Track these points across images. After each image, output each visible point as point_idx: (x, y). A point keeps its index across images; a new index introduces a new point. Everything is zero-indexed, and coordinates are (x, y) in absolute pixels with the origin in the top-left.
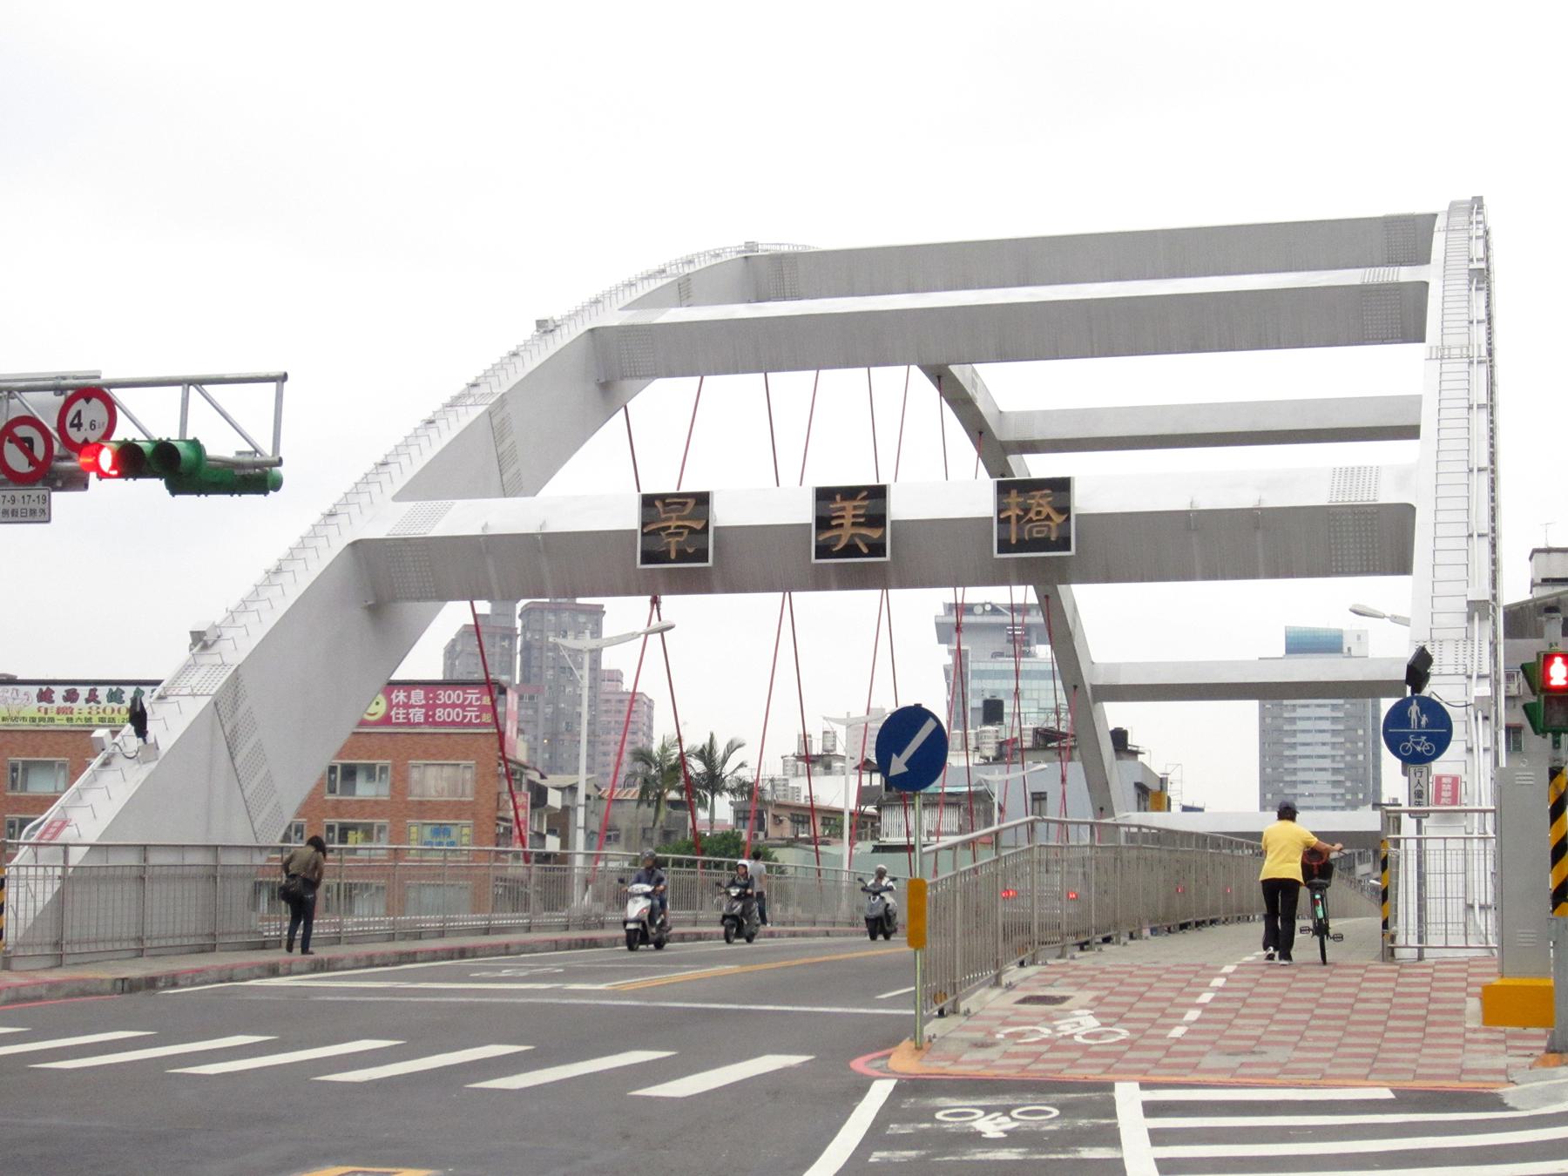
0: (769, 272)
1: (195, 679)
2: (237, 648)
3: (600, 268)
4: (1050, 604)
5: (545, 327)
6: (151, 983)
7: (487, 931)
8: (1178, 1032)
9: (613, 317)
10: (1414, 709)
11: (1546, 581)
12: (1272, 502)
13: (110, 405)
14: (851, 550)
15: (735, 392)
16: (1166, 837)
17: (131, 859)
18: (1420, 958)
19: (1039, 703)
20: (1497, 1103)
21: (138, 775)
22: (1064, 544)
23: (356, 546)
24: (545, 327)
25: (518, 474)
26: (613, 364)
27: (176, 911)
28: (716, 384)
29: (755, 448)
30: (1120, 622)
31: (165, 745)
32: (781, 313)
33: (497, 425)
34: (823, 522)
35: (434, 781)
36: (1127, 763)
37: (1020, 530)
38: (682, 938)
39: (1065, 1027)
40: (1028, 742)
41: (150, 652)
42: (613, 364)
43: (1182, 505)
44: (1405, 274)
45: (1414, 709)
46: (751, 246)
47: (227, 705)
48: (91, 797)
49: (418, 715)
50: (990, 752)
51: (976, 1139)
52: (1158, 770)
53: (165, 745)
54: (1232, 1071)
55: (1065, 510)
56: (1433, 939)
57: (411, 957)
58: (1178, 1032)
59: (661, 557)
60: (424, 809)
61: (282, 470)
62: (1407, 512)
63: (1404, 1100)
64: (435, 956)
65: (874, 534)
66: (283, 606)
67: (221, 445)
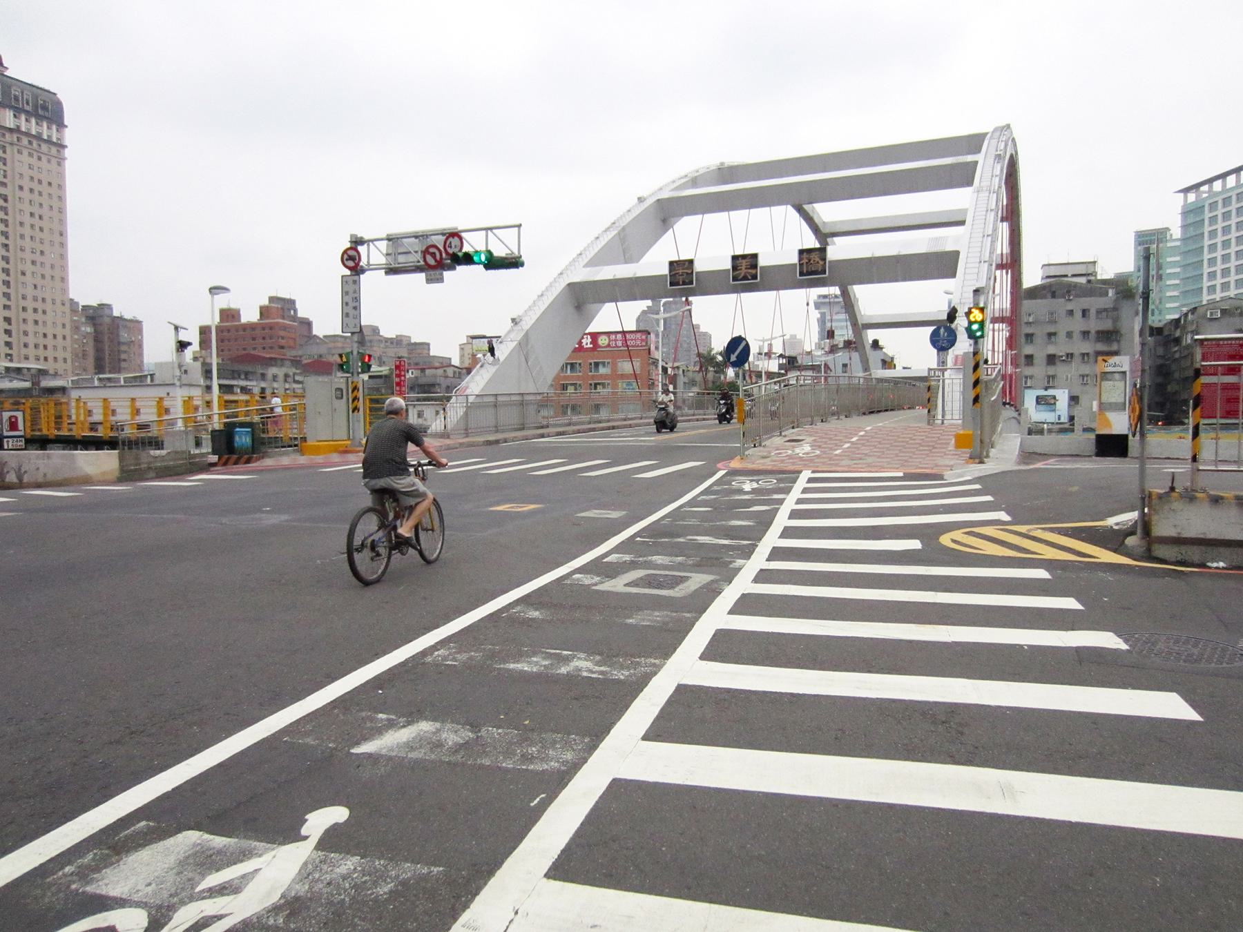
0: (727, 173)
1: (512, 336)
2: (527, 324)
3: (660, 177)
4: (845, 293)
5: (640, 200)
6: (497, 442)
7: (569, 424)
8: (838, 452)
9: (666, 195)
10: (942, 330)
11: (1048, 277)
12: (904, 252)
13: (461, 239)
14: (745, 278)
15: (717, 220)
16: (896, 382)
17: (492, 399)
19: (844, 334)
20: (941, 477)
21: (493, 369)
23: (569, 285)
24: (640, 200)
26: (666, 212)
27: (509, 417)
28: (709, 217)
29: (709, 242)
30: (873, 299)
31: (502, 359)
32: (733, 189)
33: (622, 236)
34: (735, 268)
35: (626, 367)
36: (878, 352)
38: (649, 424)
39: (797, 451)
40: (841, 345)
41: (496, 326)
42: (666, 212)
43: (868, 255)
44: (970, 158)
45: (942, 330)
46: (722, 164)
47: (524, 345)
48: (478, 378)
49: (620, 343)
50: (827, 349)
51: (741, 491)
52: (890, 355)
53: (502, 359)
54: (849, 466)
55: (824, 259)
56: (948, 417)
57: (594, 430)
58: (838, 452)
59: (678, 284)
60: (623, 376)
61: (523, 258)
62: (957, 253)
63: (907, 477)
64: (603, 429)
65: (753, 271)
66: (543, 308)
67: (499, 252)
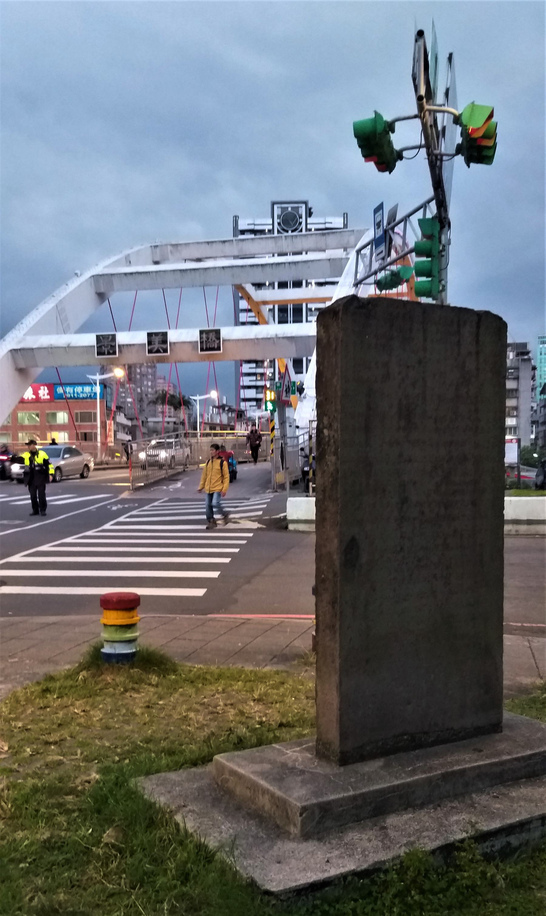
14: (158, 351)
18: (39, 507)
22: (219, 349)
25: (68, 325)
34: (150, 343)
37: (206, 345)
55: (219, 338)
59: (103, 354)
65: (164, 346)
